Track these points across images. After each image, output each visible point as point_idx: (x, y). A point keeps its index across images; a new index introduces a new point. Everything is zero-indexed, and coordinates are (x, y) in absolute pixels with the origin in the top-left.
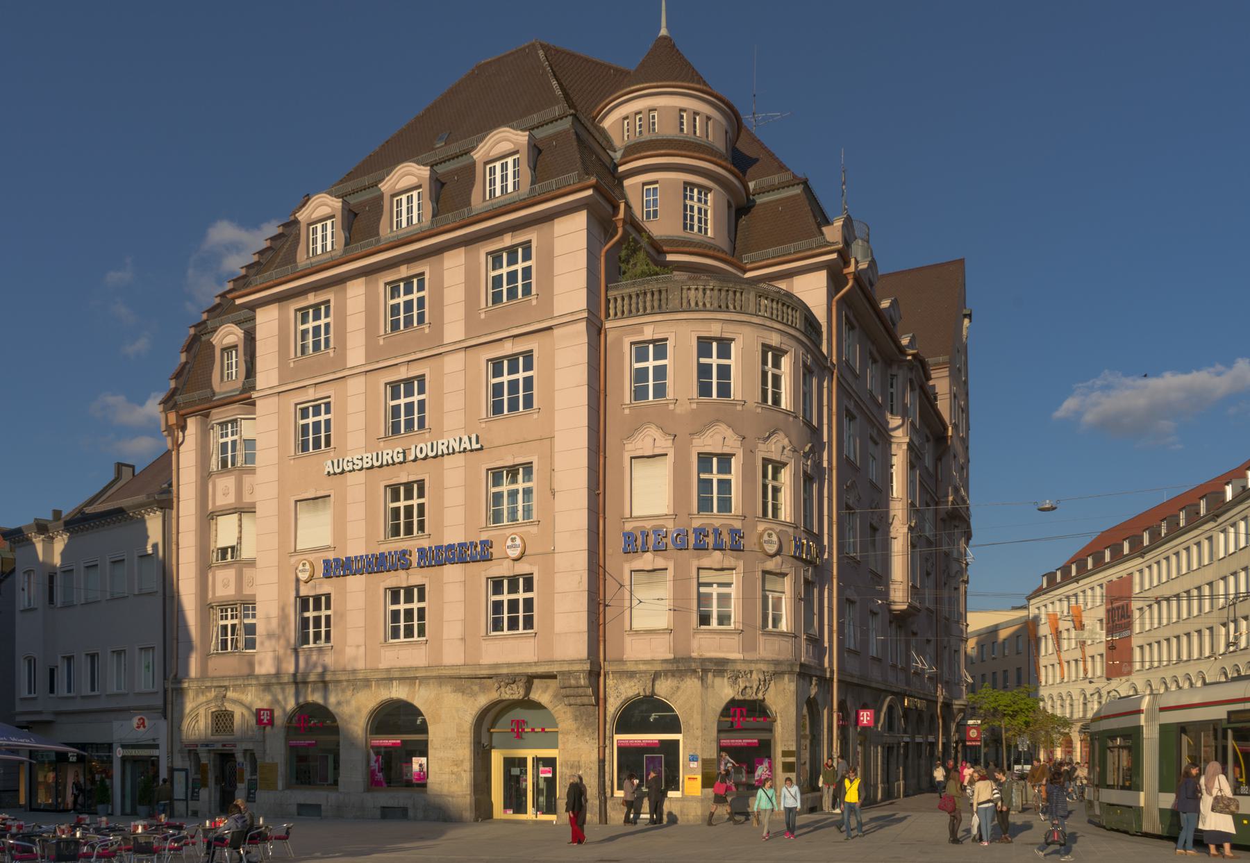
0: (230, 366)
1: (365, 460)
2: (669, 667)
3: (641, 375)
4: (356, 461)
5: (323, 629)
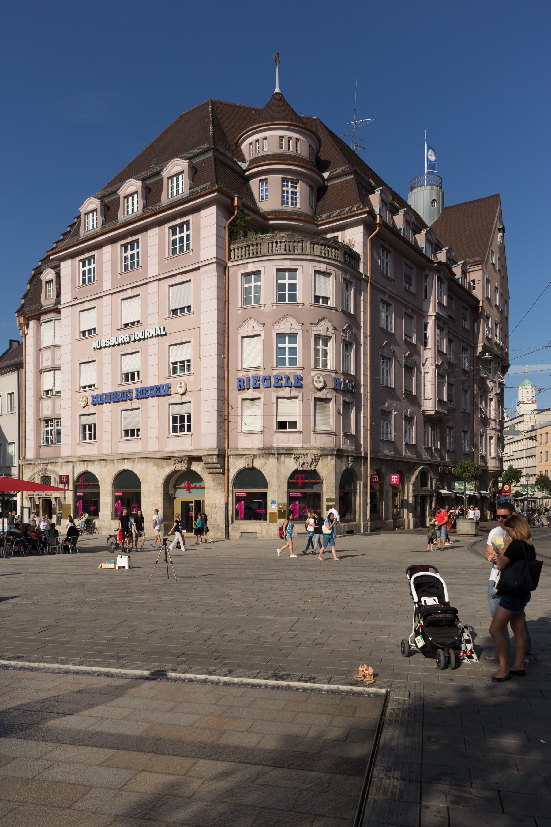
0: (50, 291)
1: (111, 341)
2: (260, 452)
3: (247, 291)
4: (107, 342)
5: (186, 424)
